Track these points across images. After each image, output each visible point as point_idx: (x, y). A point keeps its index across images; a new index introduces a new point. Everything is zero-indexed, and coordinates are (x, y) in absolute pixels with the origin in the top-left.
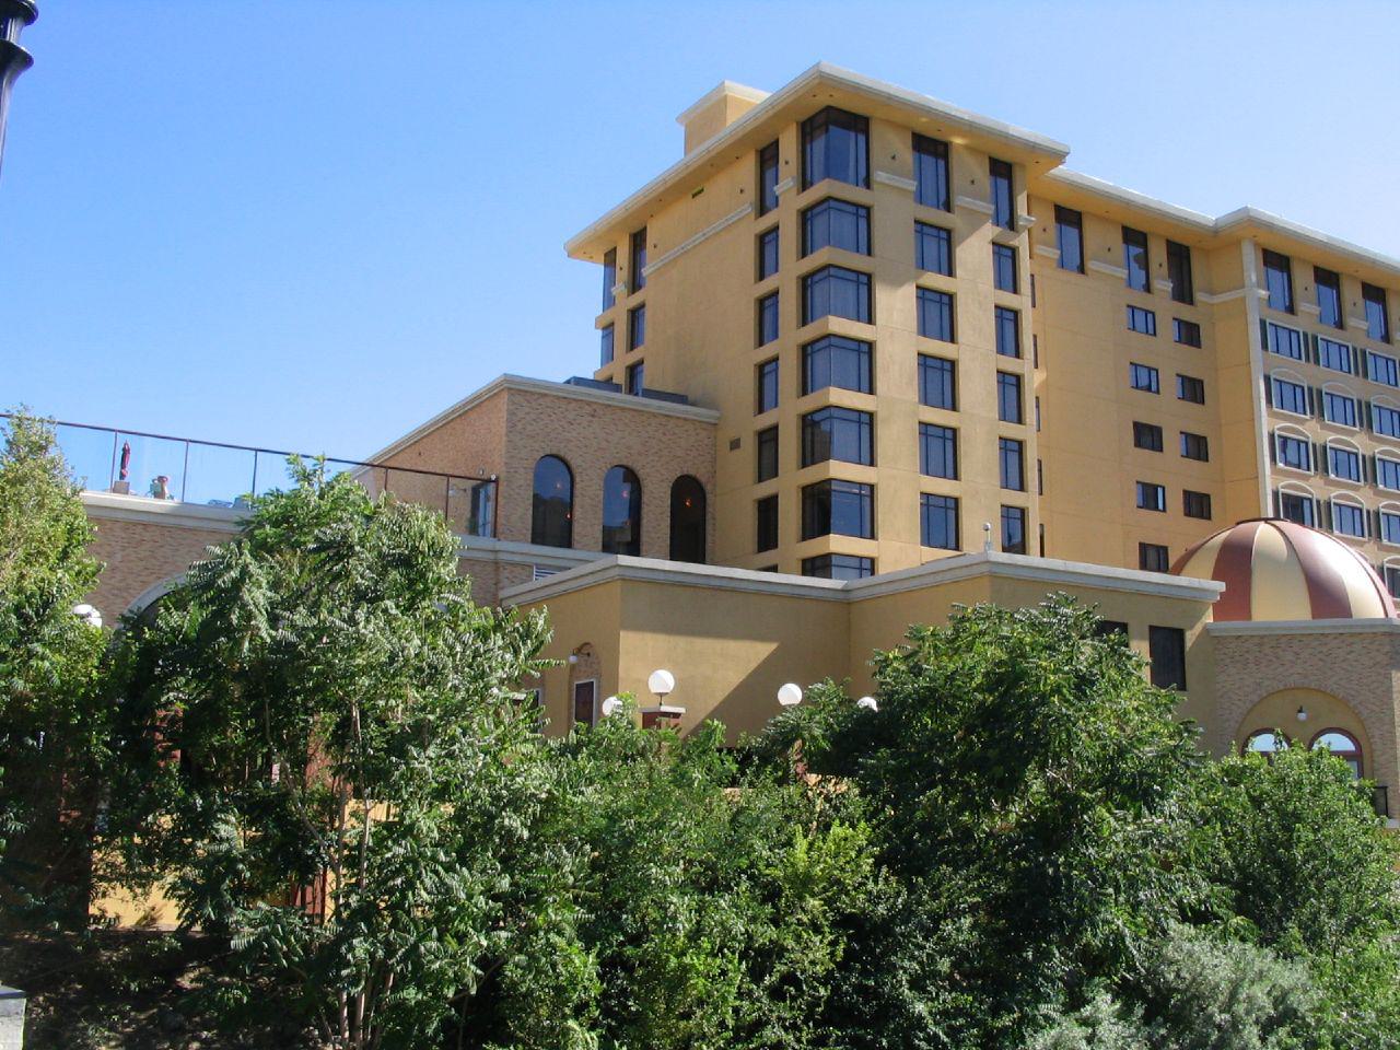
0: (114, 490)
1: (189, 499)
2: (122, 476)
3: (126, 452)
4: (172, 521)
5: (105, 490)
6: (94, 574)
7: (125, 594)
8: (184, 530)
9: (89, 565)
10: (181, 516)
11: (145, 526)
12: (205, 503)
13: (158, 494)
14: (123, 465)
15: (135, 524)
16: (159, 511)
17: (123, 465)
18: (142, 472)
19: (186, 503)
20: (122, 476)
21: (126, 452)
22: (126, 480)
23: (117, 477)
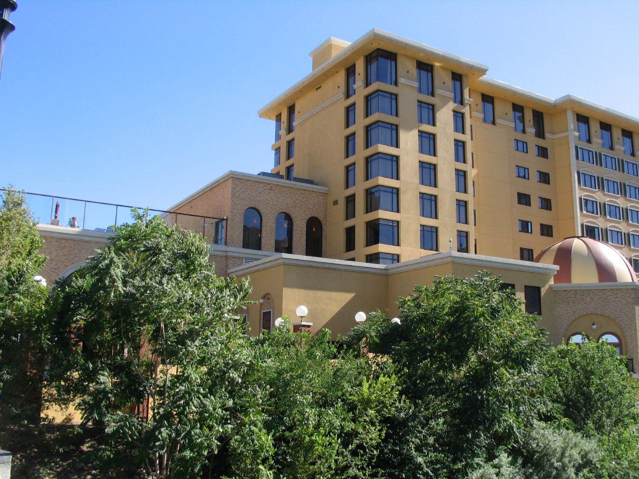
0: (52, 224)
1: (86, 228)
2: (56, 217)
3: (57, 206)
4: (79, 238)
5: (48, 224)
6: (43, 262)
7: (57, 271)
8: (84, 242)
9: (41, 258)
10: (83, 236)
11: (66, 240)
12: (94, 229)
13: (72, 225)
14: (56, 212)
15: (62, 239)
16: (73, 233)
17: (56, 212)
18: (65, 215)
19: (85, 230)
20: (56, 217)
21: (57, 206)
22: (58, 219)
23: (53, 218)
